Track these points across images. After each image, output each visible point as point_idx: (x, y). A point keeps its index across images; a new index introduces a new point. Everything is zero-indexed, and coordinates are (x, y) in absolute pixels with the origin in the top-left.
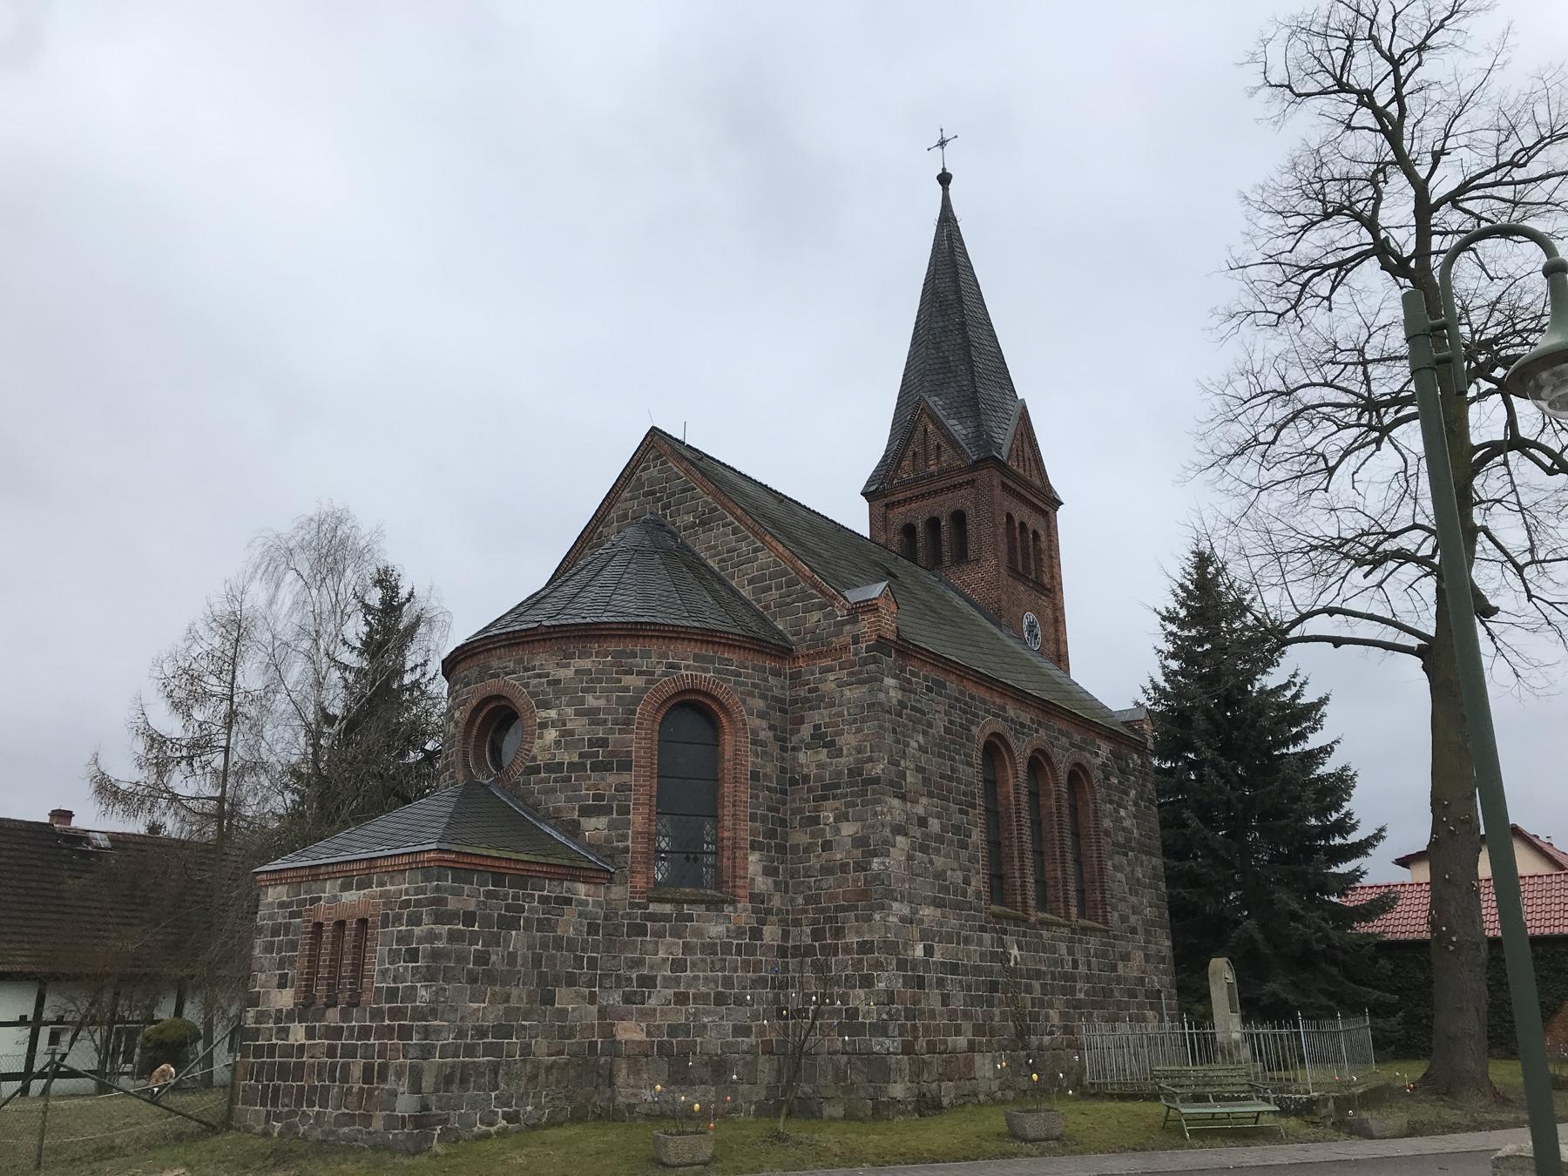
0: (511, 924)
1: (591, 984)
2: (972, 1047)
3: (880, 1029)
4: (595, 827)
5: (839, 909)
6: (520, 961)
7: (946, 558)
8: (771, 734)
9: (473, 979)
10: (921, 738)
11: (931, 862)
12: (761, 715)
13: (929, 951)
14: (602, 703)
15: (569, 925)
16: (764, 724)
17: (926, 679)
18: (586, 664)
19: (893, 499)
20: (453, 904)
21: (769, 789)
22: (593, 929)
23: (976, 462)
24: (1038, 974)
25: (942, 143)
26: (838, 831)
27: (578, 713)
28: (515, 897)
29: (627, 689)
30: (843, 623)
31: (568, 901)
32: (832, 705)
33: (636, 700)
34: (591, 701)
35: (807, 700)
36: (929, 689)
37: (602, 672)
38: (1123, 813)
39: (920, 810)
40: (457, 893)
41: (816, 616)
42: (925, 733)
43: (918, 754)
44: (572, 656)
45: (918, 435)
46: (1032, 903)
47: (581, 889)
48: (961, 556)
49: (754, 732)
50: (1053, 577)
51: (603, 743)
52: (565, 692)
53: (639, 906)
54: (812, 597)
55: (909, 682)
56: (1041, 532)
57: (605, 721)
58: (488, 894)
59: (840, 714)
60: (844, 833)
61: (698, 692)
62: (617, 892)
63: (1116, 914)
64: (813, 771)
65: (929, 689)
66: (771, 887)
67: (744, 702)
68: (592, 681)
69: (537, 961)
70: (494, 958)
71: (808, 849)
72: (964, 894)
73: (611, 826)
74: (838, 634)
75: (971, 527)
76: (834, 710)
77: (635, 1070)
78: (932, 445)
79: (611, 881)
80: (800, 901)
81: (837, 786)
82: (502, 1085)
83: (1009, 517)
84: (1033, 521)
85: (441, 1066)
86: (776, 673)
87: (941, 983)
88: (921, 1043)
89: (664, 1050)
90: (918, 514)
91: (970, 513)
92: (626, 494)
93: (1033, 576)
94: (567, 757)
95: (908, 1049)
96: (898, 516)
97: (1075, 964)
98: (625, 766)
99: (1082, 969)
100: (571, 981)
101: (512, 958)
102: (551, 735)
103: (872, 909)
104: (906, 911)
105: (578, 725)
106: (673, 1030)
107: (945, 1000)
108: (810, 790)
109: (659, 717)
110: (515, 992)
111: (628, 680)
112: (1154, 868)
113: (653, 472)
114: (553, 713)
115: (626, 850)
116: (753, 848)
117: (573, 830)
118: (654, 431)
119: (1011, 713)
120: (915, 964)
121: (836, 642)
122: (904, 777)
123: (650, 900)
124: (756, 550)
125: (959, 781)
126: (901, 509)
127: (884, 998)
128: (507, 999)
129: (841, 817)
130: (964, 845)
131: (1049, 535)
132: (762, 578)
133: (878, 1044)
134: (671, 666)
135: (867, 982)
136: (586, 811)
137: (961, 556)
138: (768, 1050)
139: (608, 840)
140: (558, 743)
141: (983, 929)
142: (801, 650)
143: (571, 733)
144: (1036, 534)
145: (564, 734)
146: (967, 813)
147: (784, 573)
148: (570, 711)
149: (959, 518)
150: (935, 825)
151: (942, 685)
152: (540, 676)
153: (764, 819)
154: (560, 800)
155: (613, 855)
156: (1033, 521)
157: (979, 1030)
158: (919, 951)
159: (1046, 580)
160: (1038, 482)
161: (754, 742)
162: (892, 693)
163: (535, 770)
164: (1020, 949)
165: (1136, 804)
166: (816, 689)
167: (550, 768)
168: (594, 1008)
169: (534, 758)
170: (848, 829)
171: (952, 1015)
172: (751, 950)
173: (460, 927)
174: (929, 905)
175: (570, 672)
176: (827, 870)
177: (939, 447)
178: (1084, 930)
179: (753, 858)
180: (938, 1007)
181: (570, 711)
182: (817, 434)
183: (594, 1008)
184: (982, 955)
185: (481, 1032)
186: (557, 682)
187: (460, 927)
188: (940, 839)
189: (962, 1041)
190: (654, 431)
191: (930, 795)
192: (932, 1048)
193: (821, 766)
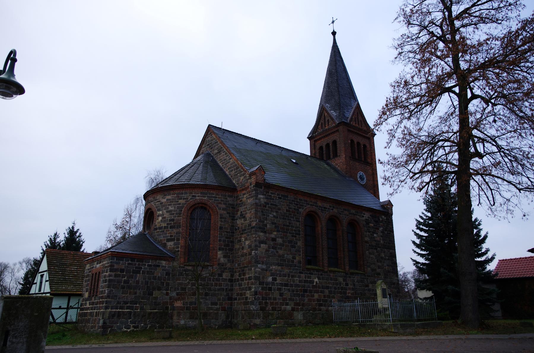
0: (138, 272)
1: (167, 290)
2: (293, 309)
3: (252, 303)
4: (170, 244)
5: (245, 267)
6: (140, 283)
7: (332, 156)
8: (228, 215)
9: (123, 287)
10: (275, 214)
11: (277, 252)
12: (224, 209)
13: (274, 279)
14: (173, 209)
15: (158, 273)
16: (225, 212)
17: (278, 195)
18: (169, 197)
19: (316, 139)
20: (116, 266)
21: (227, 232)
22: (168, 274)
23: (338, 124)
24: (327, 288)
25: (333, 22)
26: (245, 243)
27: (167, 212)
28: (139, 265)
29: (180, 204)
30: (248, 179)
31: (159, 266)
32: (245, 205)
33: (182, 207)
34: (171, 208)
35: (239, 204)
36: (280, 198)
37: (174, 199)
38: (375, 235)
39: (273, 236)
40: (117, 263)
41: (242, 178)
42: (276, 212)
43: (273, 219)
44: (165, 195)
45: (323, 117)
46: (326, 265)
47: (164, 263)
48: (336, 155)
49: (221, 215)
50: (372, 159)
51: (173, 220)
52: (164, 206)
53: (182, 267)
54: (242, 172)
55: (271, 196)
56: (368, 145)
57: (174, 214)
58: (129, 264)
59: (246, 208)
60: (246, 244)
61: (203, 204)
62: (175, 264)
63: (369, 269)
64: (240, 226)
65: (279, 198)
66: (226, 261)
67: (217, 206)
68: (170, 202)
69: (147, 283)
70: (131, 282)
71: (239, 249)
72: (293, 262)
73: (174, 244)
74: (247, 182)
75: (338, 145)
76: (245, 207)
77: (179, 315)
78: (327, 119)
79: (174, 260)
80: (237, 265)
81: (245, 230)
82: (132, 318)
83: (352, 141)
84: (362, 141)
85: (110, 312)
86: (230, 196)
87: (279, 289)
88: (269, 307)
89: (188, 308)
90: (323, 143)
91: (338, 141)
92: (203, 146)
93: (363, 159)
94: (164, 225)
95: (262, 309)
96: (318, 145)
97: (347, 284)
98: (179, 226)
99: (350, 286)
100: (159, 289)
101: (138, 282)
102: (160, 218)
103: (252, 266)
104: (264, 267)
105: (166, 215)
106: (191, 303)
107: (281, 295)
108: (240, 232)
109: (190, 212)
110: (138, 291)
111: (180, 201)
112: (117, 236)
113: (209, 138)
114: (161, 212)
115: (178, 251)
116: (220, 249)
117: (165, 246)
118: (210, 126)
119: (320, 204)
120: (267, 284)
121: (247, 185)
122: (266, 226)
123: (185, 265)
124: (230, 159)
125: (292, 226)
126: (319, 142)
127: (253, 294)
128: (136, 293)
129: (246, 239)
130: (293, 247)
131: (370, 145)
132: (231, 168)
133: (252, 307)
134: (193, 196)
135: (250, 289)
136: (168, 240)
137: (336, 155)
138: (224, 309)
139: (174, 248)
140: (161, 221)
141: (300, 273)
142: (239, 189)
143: (165, 218)
144: (365, 146)
145: (163, 218)
146: (296, 237)
147: (236, 165)
148: (165, 211)
149: (335, 143)
150: (279, 240)
151: (287, 197)
152: (158, 202)
153: (224, 241)
154: (162, 238)
155: (175, 252)
156: (362, 141)
157: (297, 304)
158: (270, 279)
159: (369, 160)
160: (365, 128)
161: (221, 218)
162: (262, 200)
163: (156, 229)
164: (319, 279)
165: (382, 232)
166: (241, 201)
167: (160, 228)
168: (168, 297)
169: (156, 226)
170: (247, 243)
171: (285, 299)
172: (218, 280)
173: (119, 273)
174: (275, 266)
175: (165, 200)
176: (242, 256)
177: (328, 120)
178: (352, 274)
179: (219, 253)
180: (278, 297)
181: (165, 211)
182: (286, 121)
183: (168, 297)
184: (300, 281)
185: (126, 303)
186: (162, 203)
187: (119, 273)
188: (282, 245)
189: (289, 308)
190: (210, 126)
191: (278, 231)
192: (274, 309)
193: (242, 224)
